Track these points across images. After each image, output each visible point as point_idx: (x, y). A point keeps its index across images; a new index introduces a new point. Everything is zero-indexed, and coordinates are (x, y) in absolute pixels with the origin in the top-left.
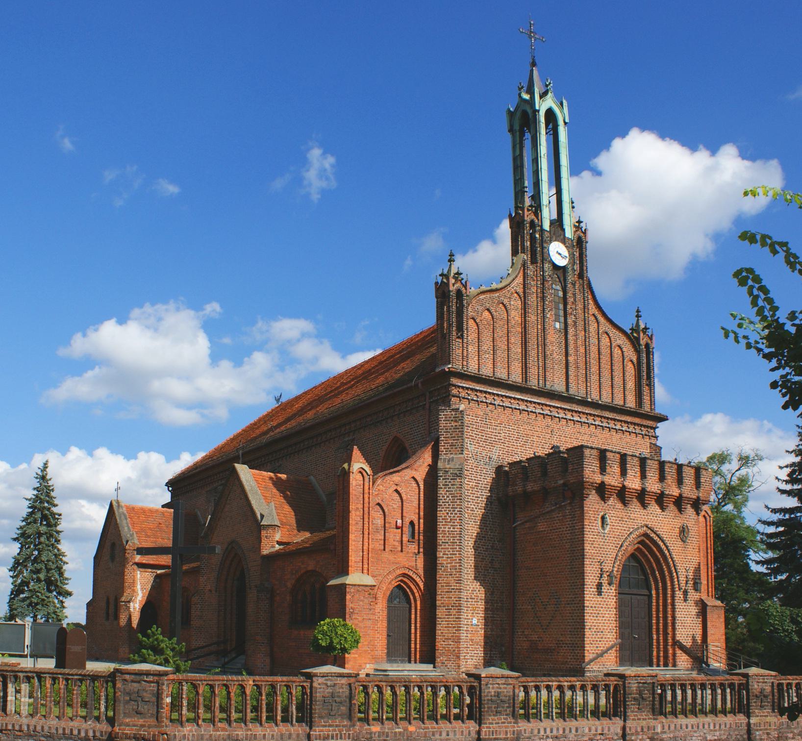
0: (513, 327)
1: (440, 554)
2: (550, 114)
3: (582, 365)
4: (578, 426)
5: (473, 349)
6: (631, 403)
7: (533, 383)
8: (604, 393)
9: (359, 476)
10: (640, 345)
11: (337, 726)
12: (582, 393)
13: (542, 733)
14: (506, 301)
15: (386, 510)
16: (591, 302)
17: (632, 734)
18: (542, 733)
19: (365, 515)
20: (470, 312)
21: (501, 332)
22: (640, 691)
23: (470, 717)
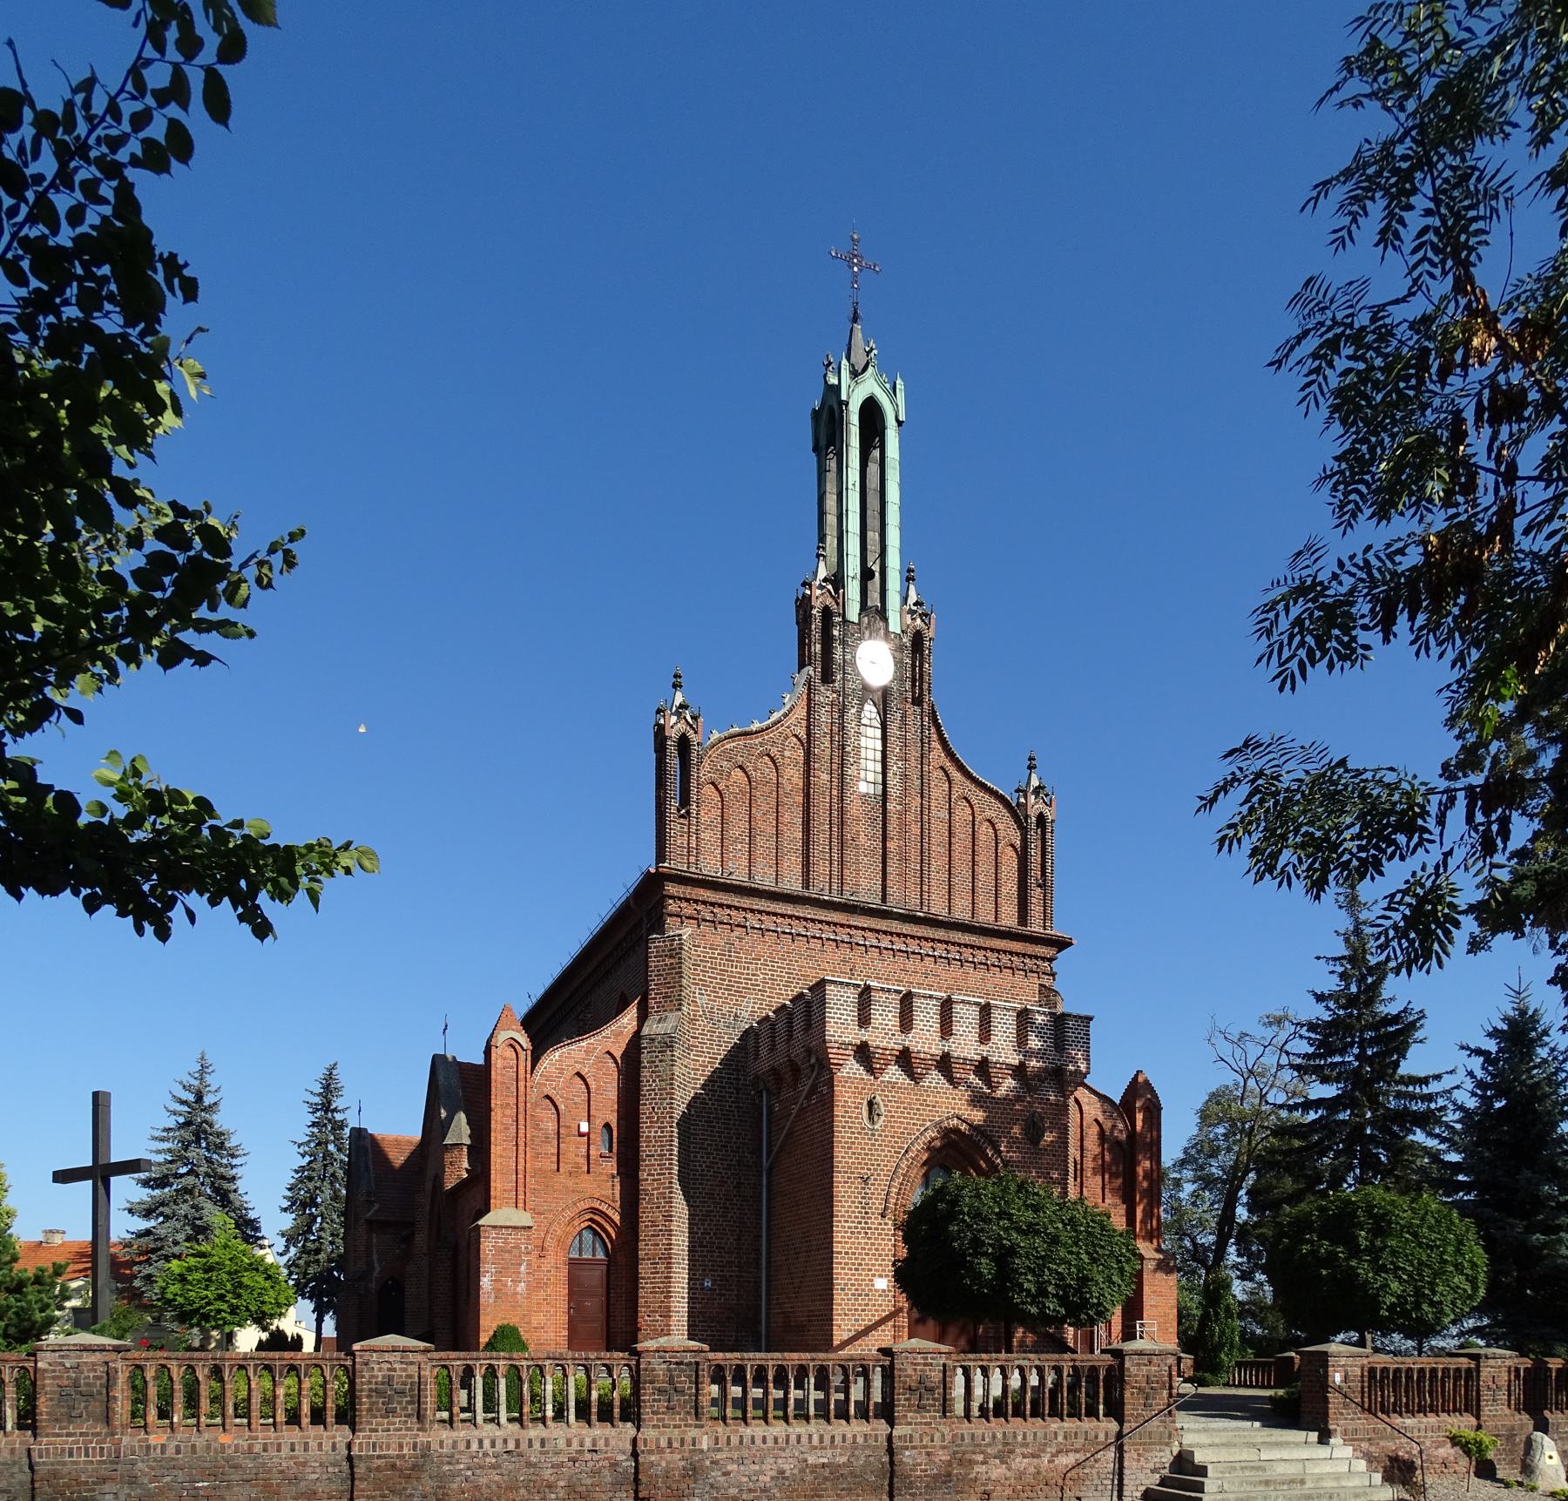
0: (787, 795)
1: (643, 1175)
2: (871, 410)
3: (914, 855)
4: (901, 958)
5: (709, 836)
6: (1009, 919)
7: (821, 887)
8: (760, 863)
9: (510, 1053)
10: (1027, 817)
11: (81, 1434)
12: (913, 902)
13: (475, 1446)
14: (774, 751)
15: (562, 1107)
16: (936, 745)
17: (651, 1452)
18: (475, 1446)
19: (520, 1114)
20: (703, 773)
21: (764, 805)
22: (671, 1377)
23: (624, 1418)
